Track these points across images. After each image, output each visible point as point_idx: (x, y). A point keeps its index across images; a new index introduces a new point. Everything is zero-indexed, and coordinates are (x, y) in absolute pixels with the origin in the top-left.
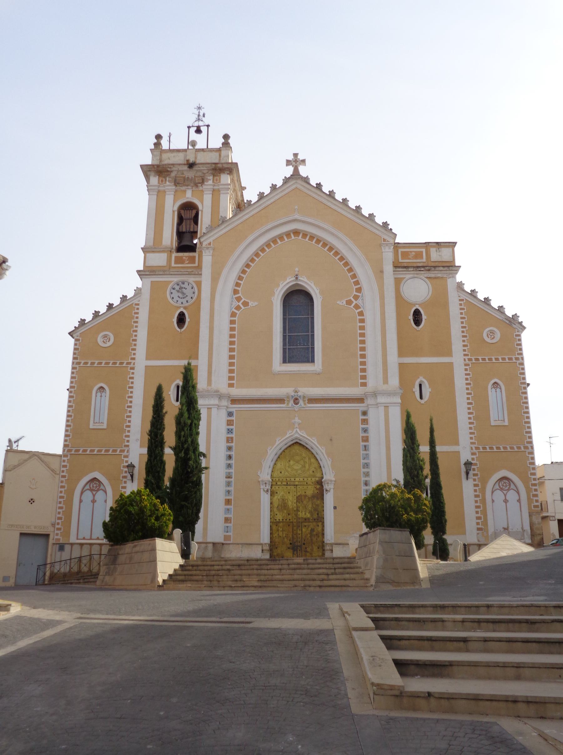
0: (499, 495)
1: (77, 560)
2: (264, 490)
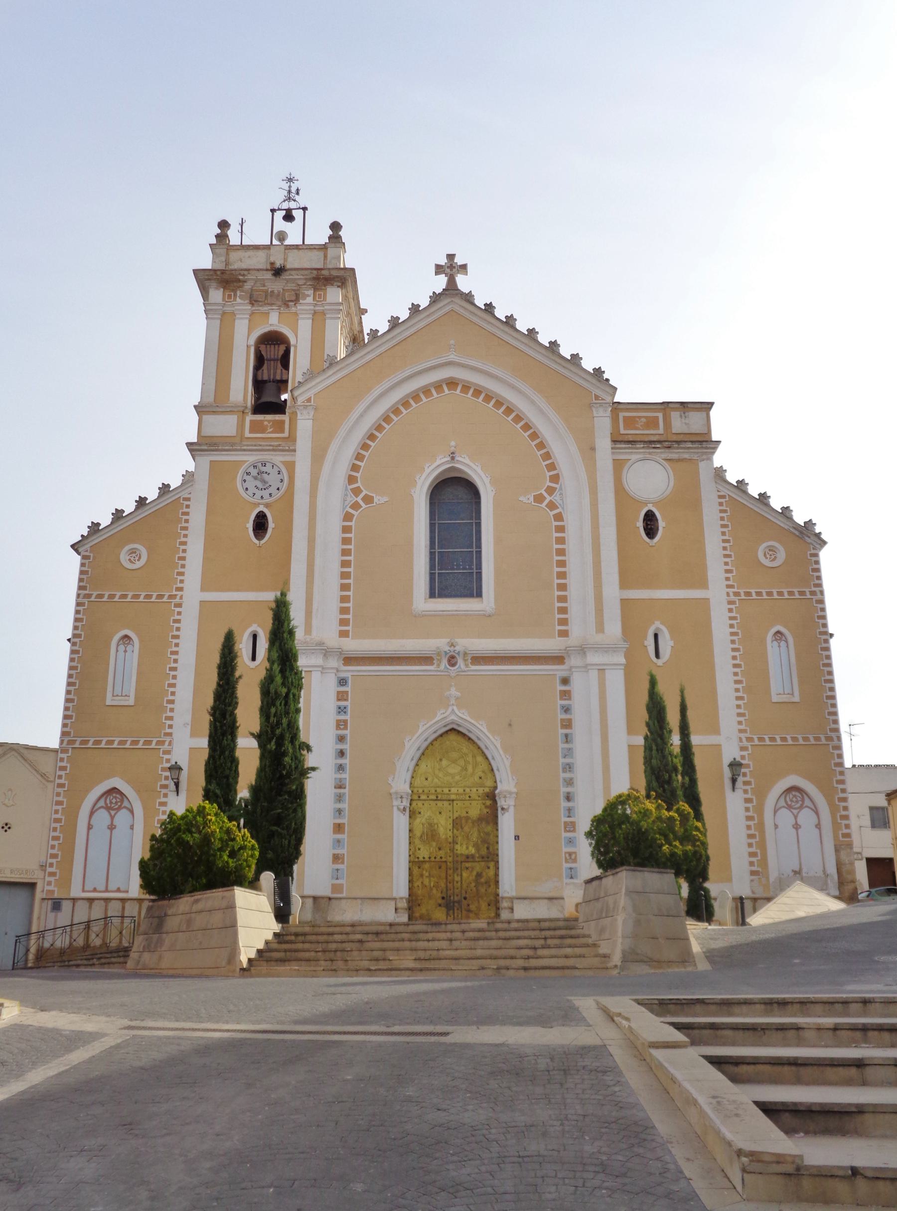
0: (785, 817)
1: (82, 926)
2: (399, 809)
